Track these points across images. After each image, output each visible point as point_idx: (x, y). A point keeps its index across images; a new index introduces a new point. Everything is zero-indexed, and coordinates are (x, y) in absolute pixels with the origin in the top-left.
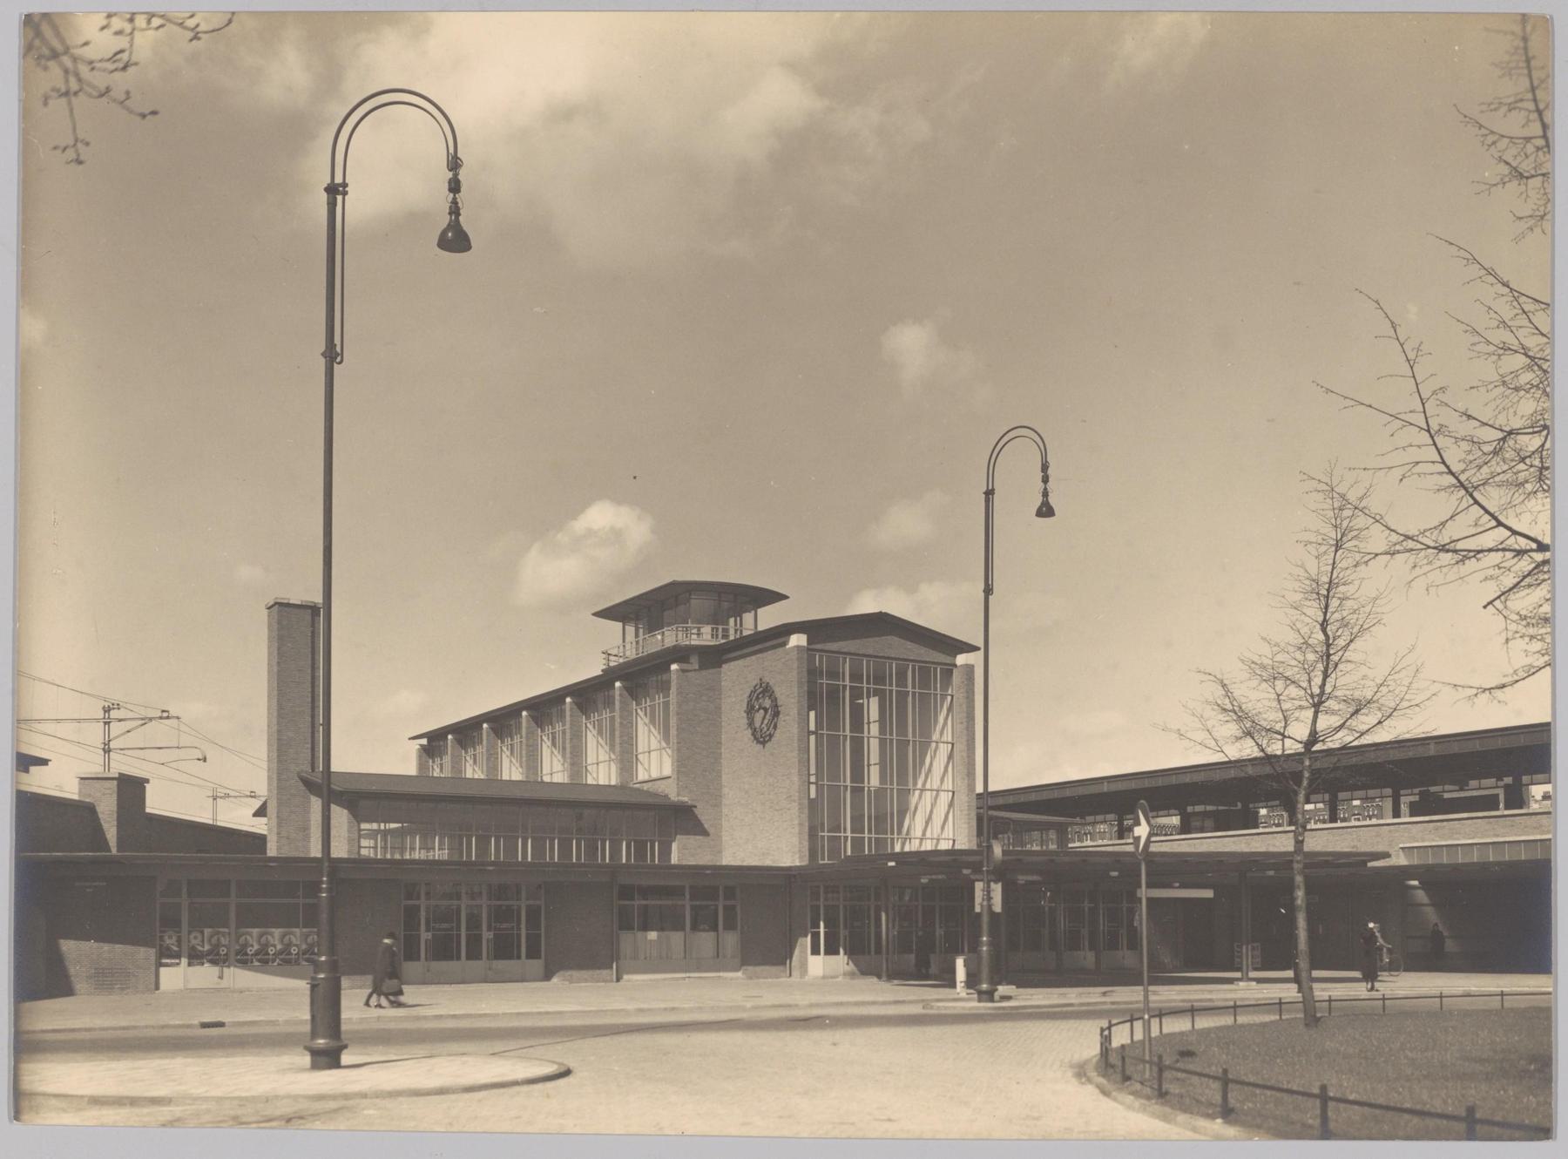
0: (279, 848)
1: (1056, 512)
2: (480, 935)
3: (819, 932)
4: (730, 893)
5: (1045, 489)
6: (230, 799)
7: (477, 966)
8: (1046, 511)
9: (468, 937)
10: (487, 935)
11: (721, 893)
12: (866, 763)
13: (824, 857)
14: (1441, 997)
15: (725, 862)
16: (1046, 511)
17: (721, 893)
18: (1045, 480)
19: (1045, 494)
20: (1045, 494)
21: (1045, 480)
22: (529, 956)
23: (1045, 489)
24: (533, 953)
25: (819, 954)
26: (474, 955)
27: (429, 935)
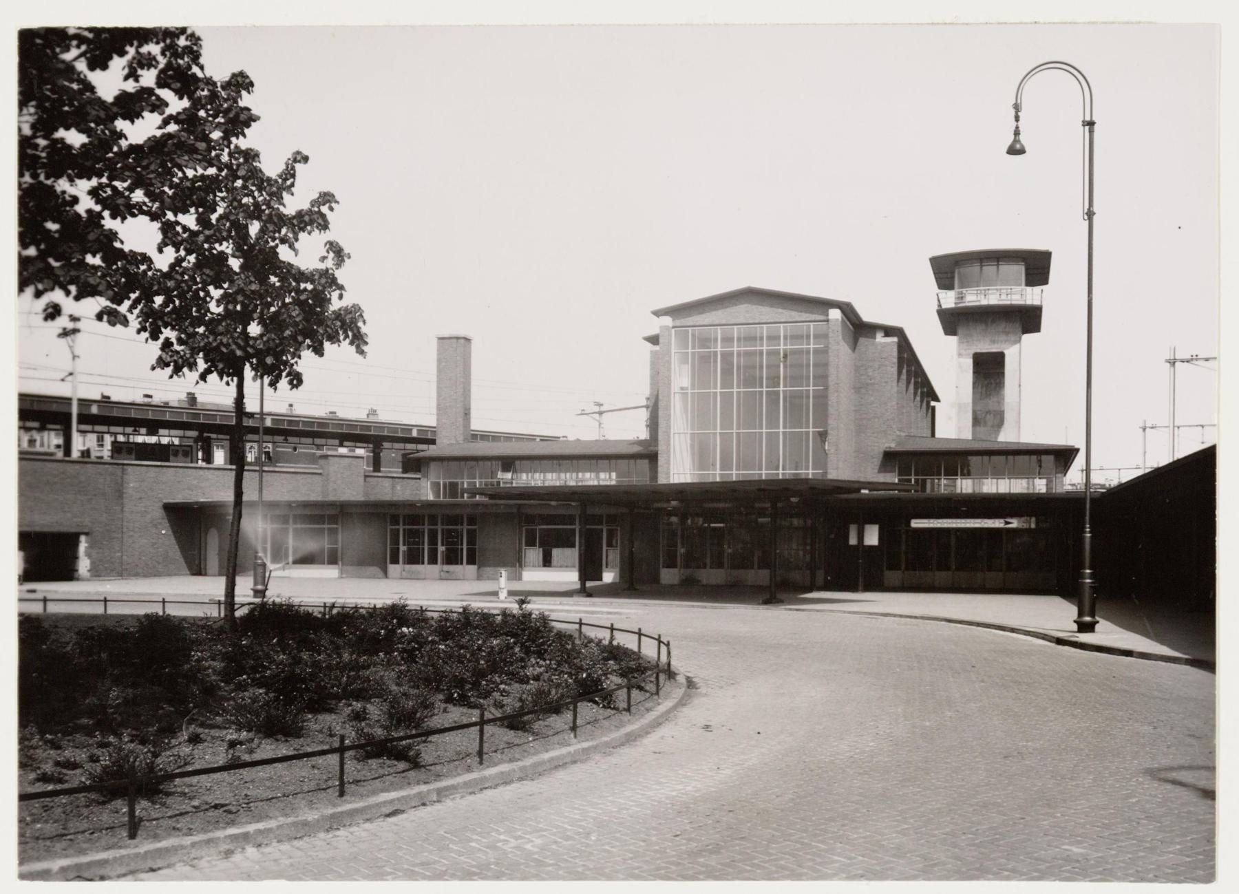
0: (702, 455)
1: (1008, 155)
2: (437, 549)
3: (467, 545)
4: (472, 520)
5: (1017, 127)
6: (1199, 362)
7: (435, 569)
8: (1015, 150)
9: (468, 550)
10: (441, 549)
11: (465, 519)
12: (126, 462)
13: (809, 466)
14: (164, 602)
15: (672, 482)
16: (1015, 150)
17: (465, 519)
18: (1017, 119)
19: (1017, 133)
20: (1017, 133)
21: (1017, 119)
22: (469, 563)
23: (1017, 127)
24: (471, 561)
25: (436, 563)
26: (433, 561)
27: (443, 548)
